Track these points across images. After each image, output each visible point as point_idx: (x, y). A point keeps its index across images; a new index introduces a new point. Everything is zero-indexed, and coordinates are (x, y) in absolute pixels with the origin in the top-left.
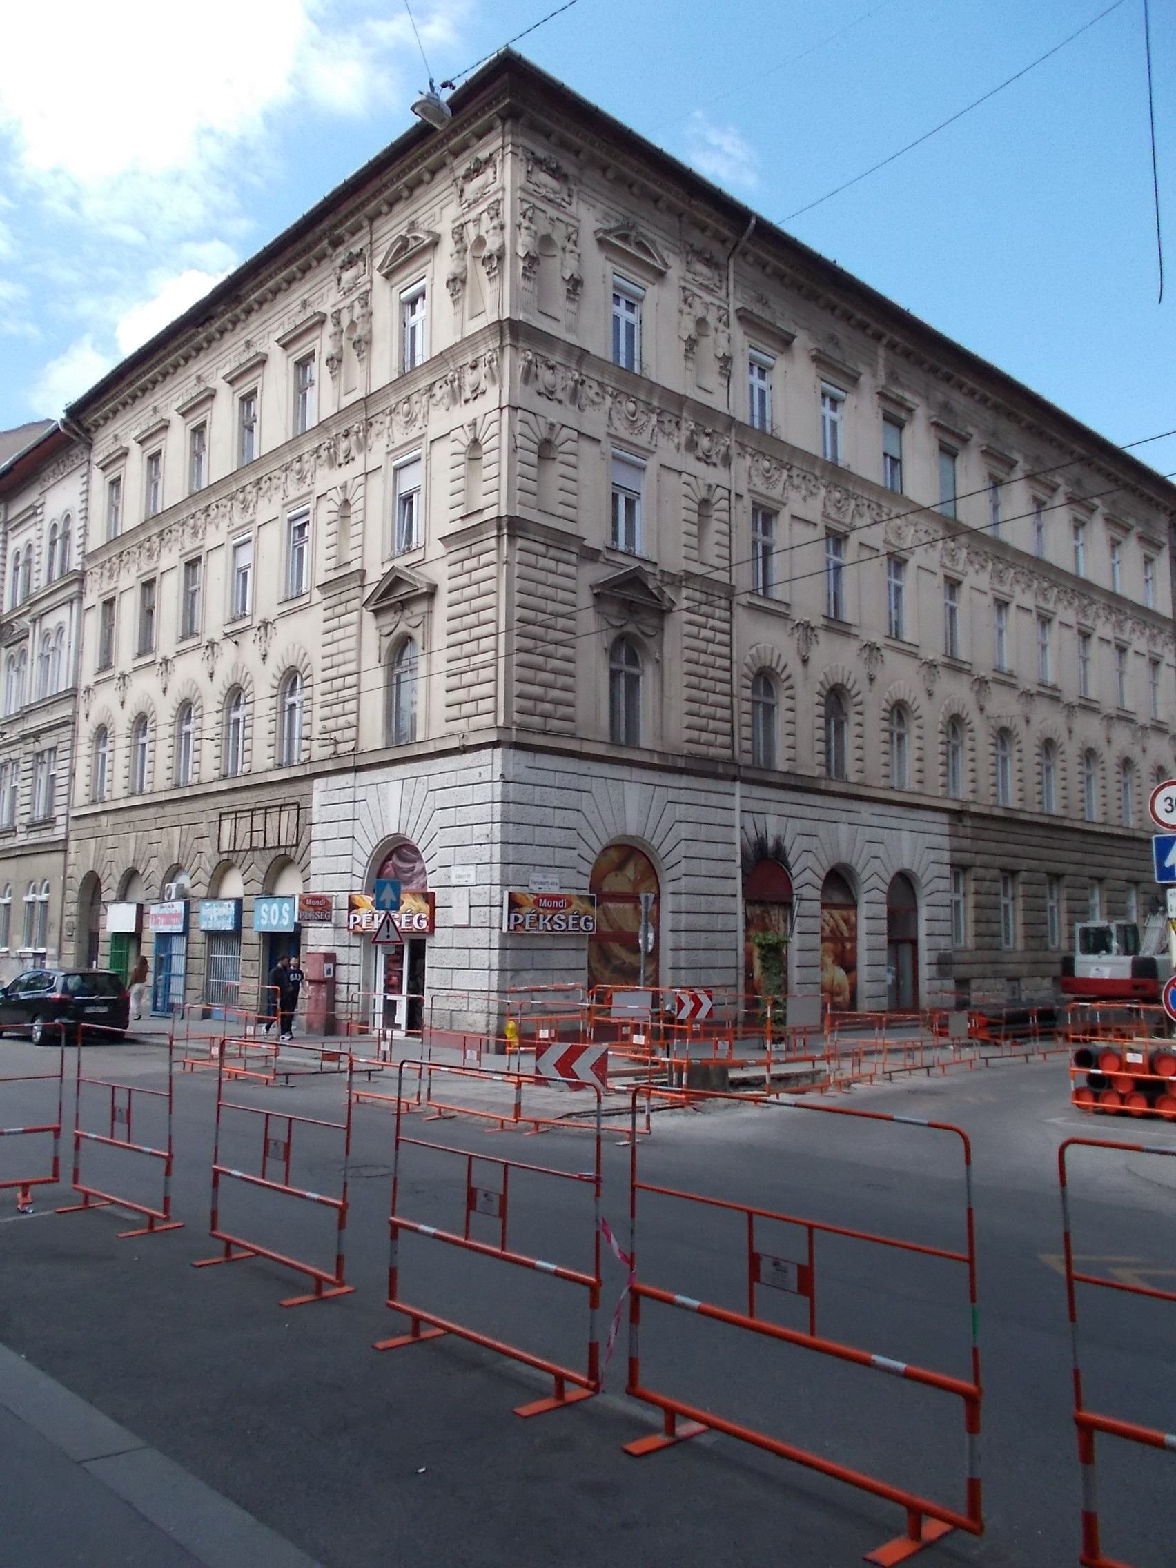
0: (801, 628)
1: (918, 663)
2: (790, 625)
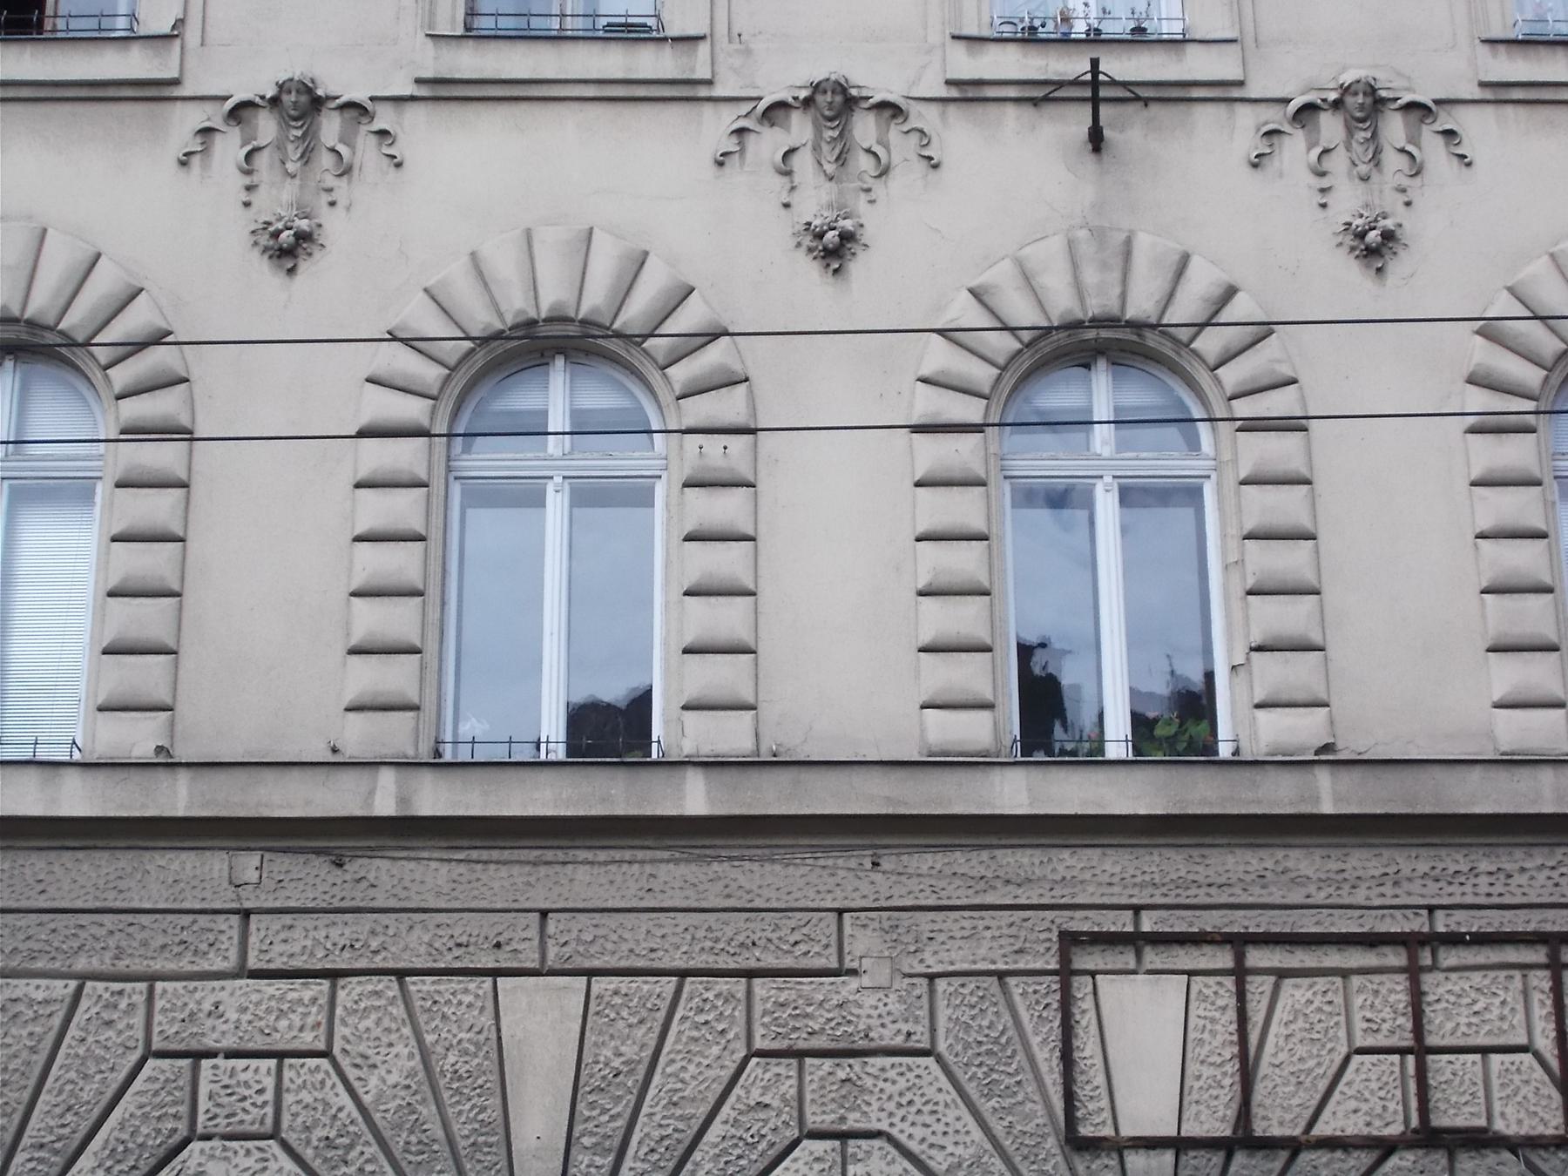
0: (1331, 127)
1: (716, 125)
2: (729, 117)
